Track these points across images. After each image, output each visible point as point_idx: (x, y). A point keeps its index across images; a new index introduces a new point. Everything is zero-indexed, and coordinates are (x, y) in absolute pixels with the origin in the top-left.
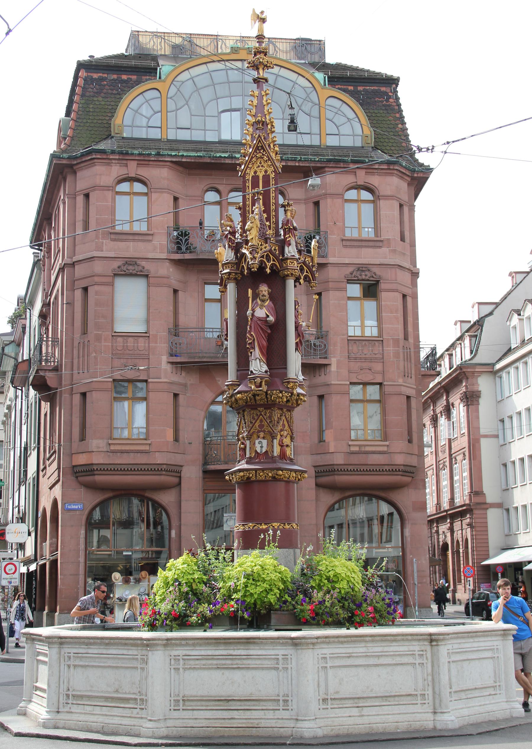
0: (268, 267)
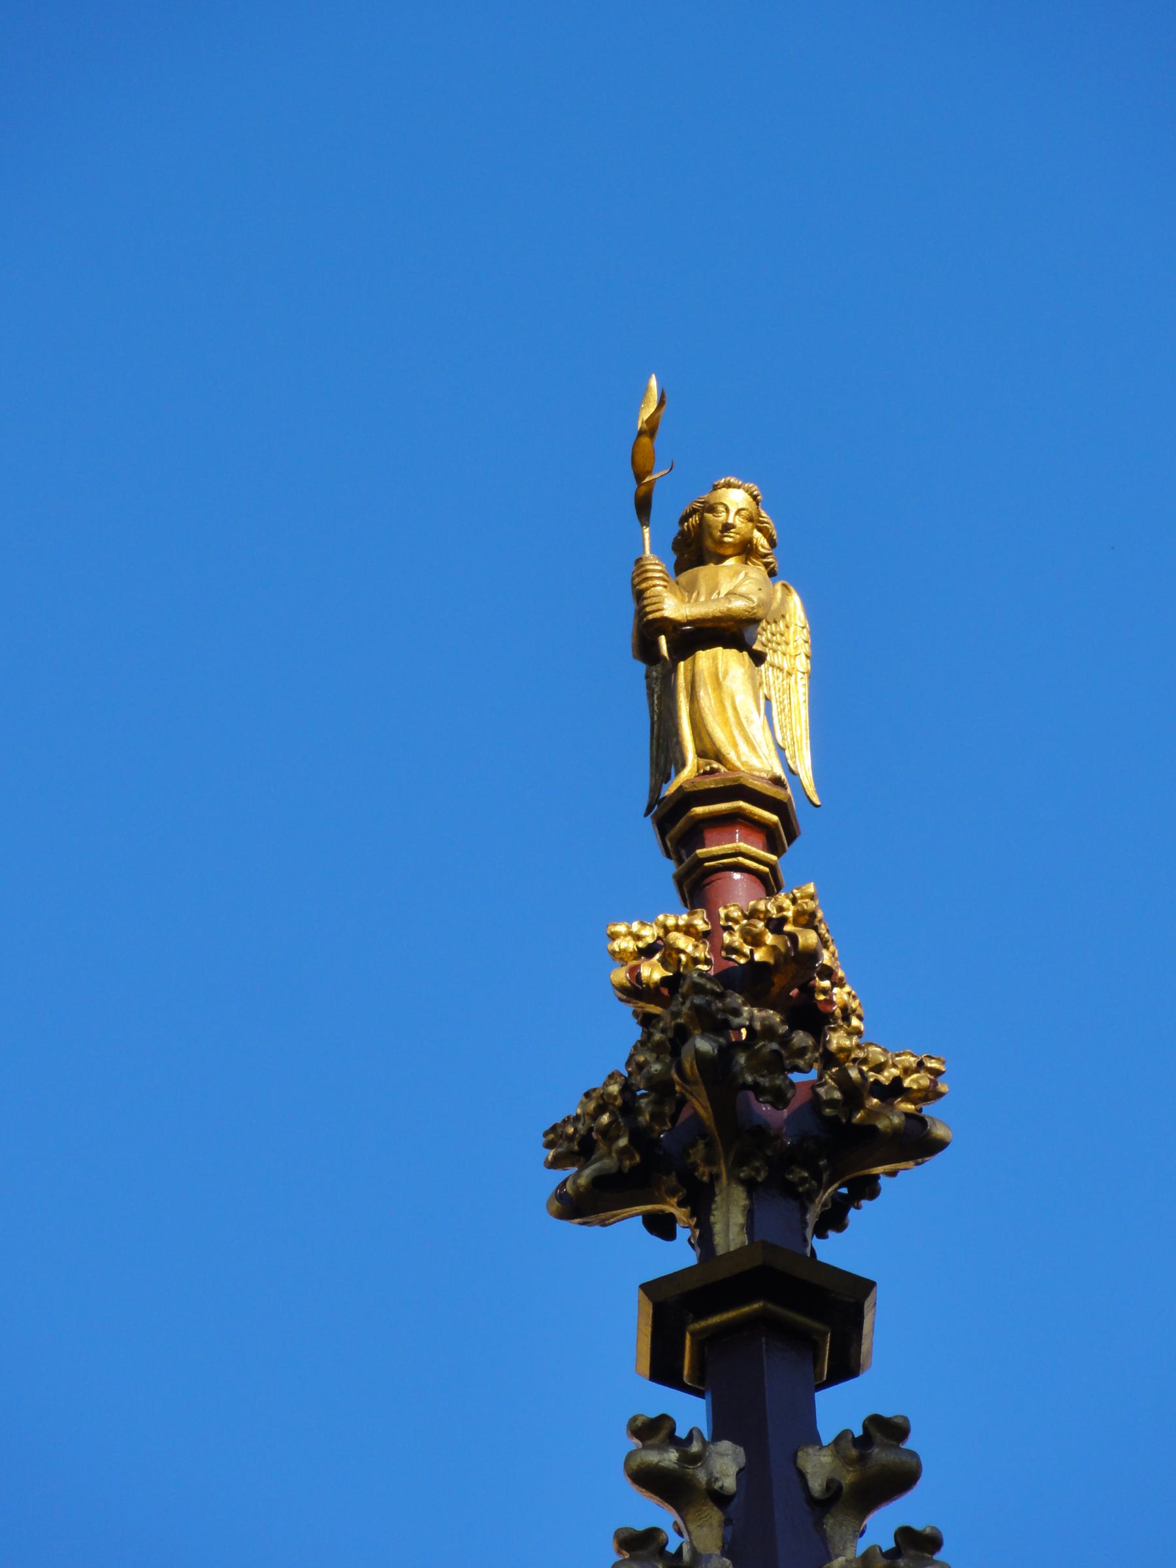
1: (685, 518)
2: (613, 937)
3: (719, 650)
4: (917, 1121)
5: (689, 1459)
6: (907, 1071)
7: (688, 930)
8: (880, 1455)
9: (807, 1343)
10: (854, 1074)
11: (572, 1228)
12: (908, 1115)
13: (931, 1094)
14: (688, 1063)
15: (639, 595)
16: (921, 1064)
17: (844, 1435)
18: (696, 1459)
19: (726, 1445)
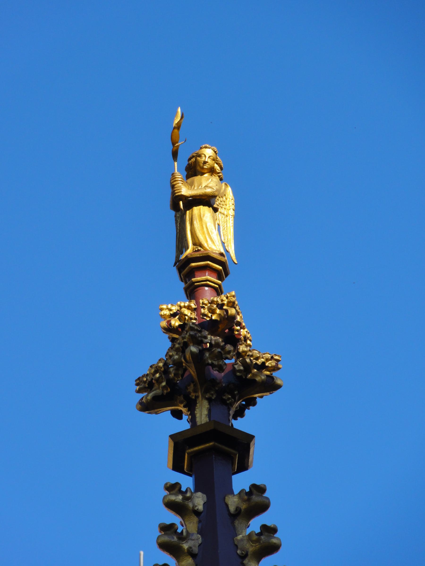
1: (190, 159)
2: (162, 310)
3: (201, 207)
4: (271, 378)
5: (186, 499)
6: (267, 360)
7: (189, 308)
8: (255, 498)
9: (229, 458)
10: (248, 360)
11: (145, 414)
12: (267, 376)
13: (276, 368)
14: (188, 355)
15: (173, 187)
16: (272, 357)
18: (189, 499)
19: (199, 494)
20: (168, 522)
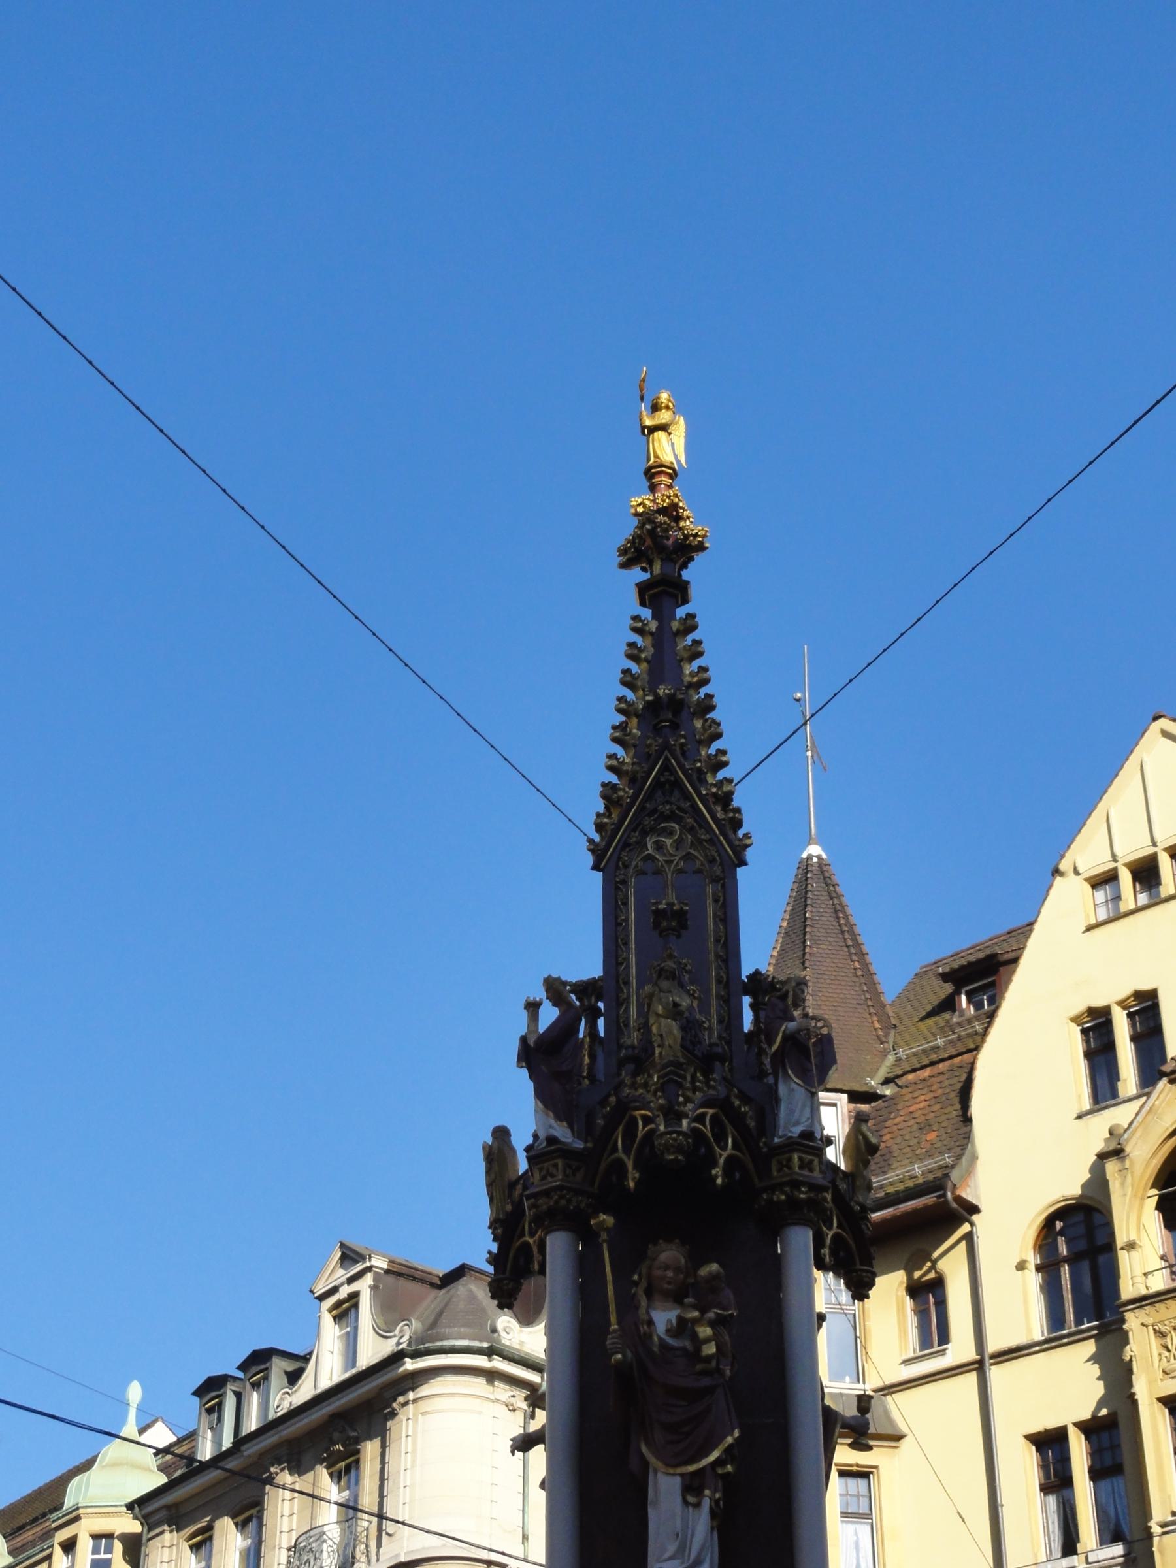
0: (722, 1161)
1: (653, 401)
2: (631, 502)
3: (660, 432)
4: (701, 543)
5: (644, 625)
6: (699, 531)
7: (649, 499)
8: (689, 622)
9: (676, 597)
10: (686, 532)
11: (623, 571)
12: (699, 541)
13: (704, 536)
14: (645, 531)
15: (641, 420)
16: (703, 529)
17: (681, 617)
18: (647, 624)
19: (654, 621)
20: (632, 641)
